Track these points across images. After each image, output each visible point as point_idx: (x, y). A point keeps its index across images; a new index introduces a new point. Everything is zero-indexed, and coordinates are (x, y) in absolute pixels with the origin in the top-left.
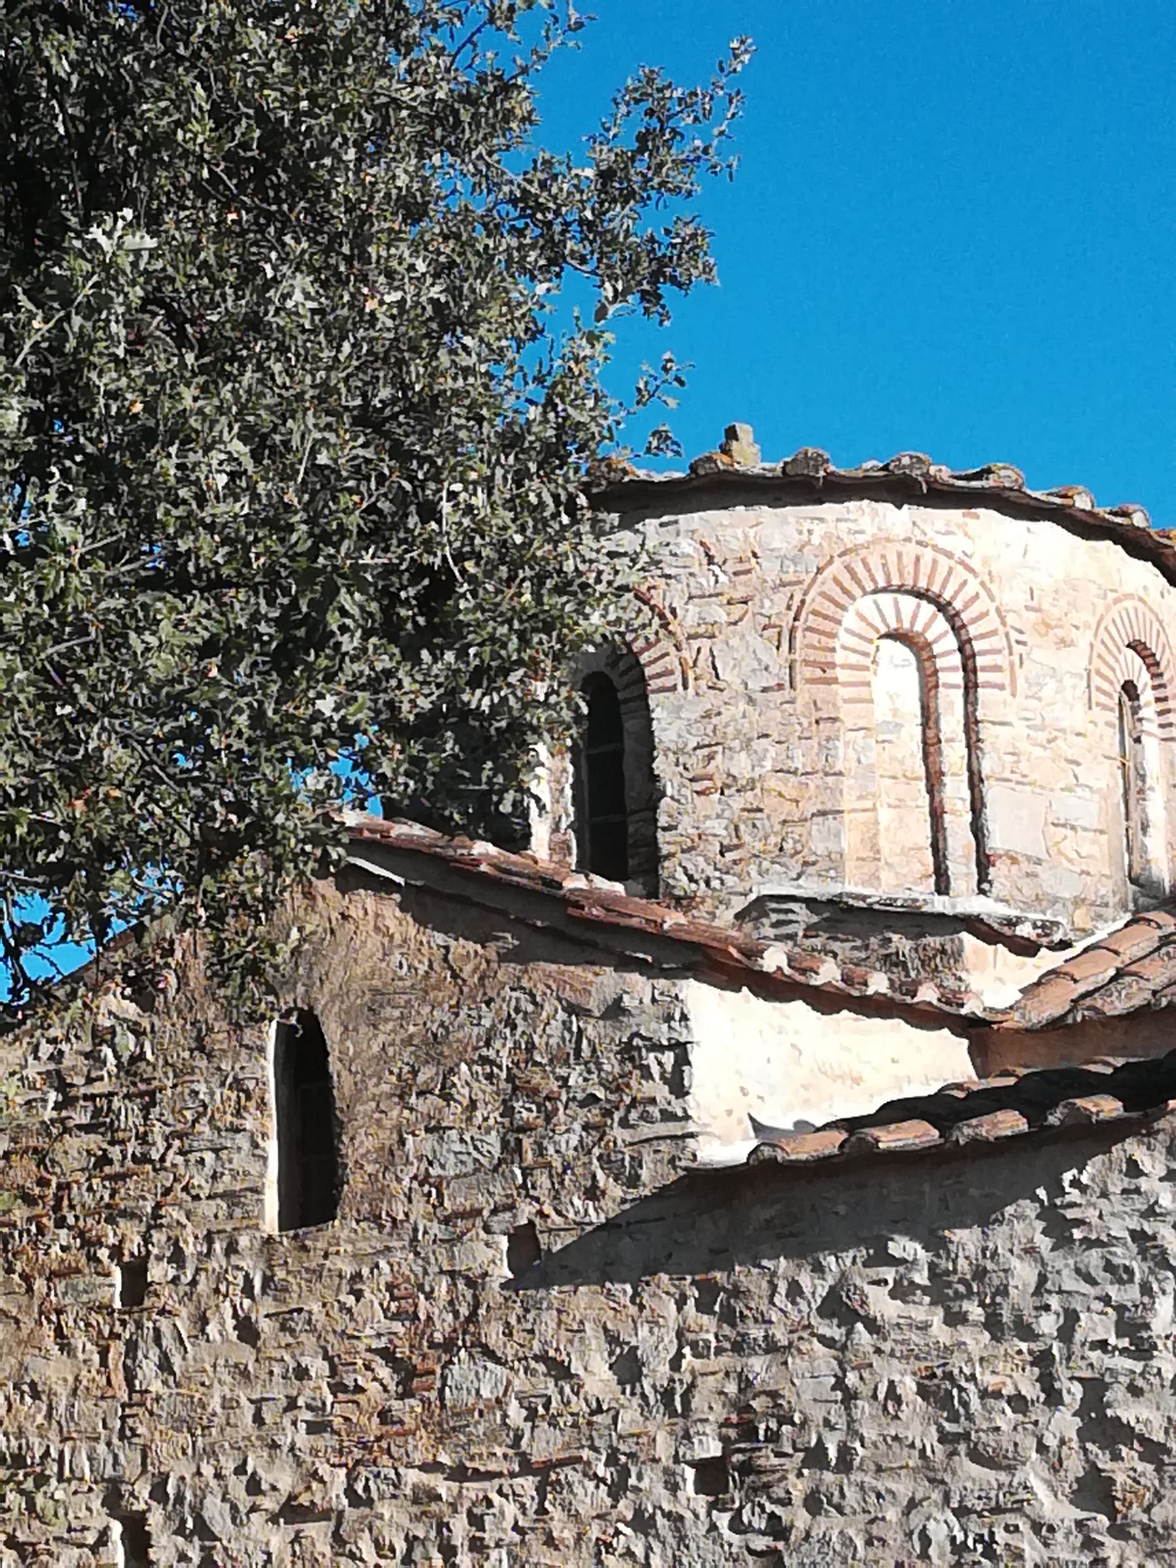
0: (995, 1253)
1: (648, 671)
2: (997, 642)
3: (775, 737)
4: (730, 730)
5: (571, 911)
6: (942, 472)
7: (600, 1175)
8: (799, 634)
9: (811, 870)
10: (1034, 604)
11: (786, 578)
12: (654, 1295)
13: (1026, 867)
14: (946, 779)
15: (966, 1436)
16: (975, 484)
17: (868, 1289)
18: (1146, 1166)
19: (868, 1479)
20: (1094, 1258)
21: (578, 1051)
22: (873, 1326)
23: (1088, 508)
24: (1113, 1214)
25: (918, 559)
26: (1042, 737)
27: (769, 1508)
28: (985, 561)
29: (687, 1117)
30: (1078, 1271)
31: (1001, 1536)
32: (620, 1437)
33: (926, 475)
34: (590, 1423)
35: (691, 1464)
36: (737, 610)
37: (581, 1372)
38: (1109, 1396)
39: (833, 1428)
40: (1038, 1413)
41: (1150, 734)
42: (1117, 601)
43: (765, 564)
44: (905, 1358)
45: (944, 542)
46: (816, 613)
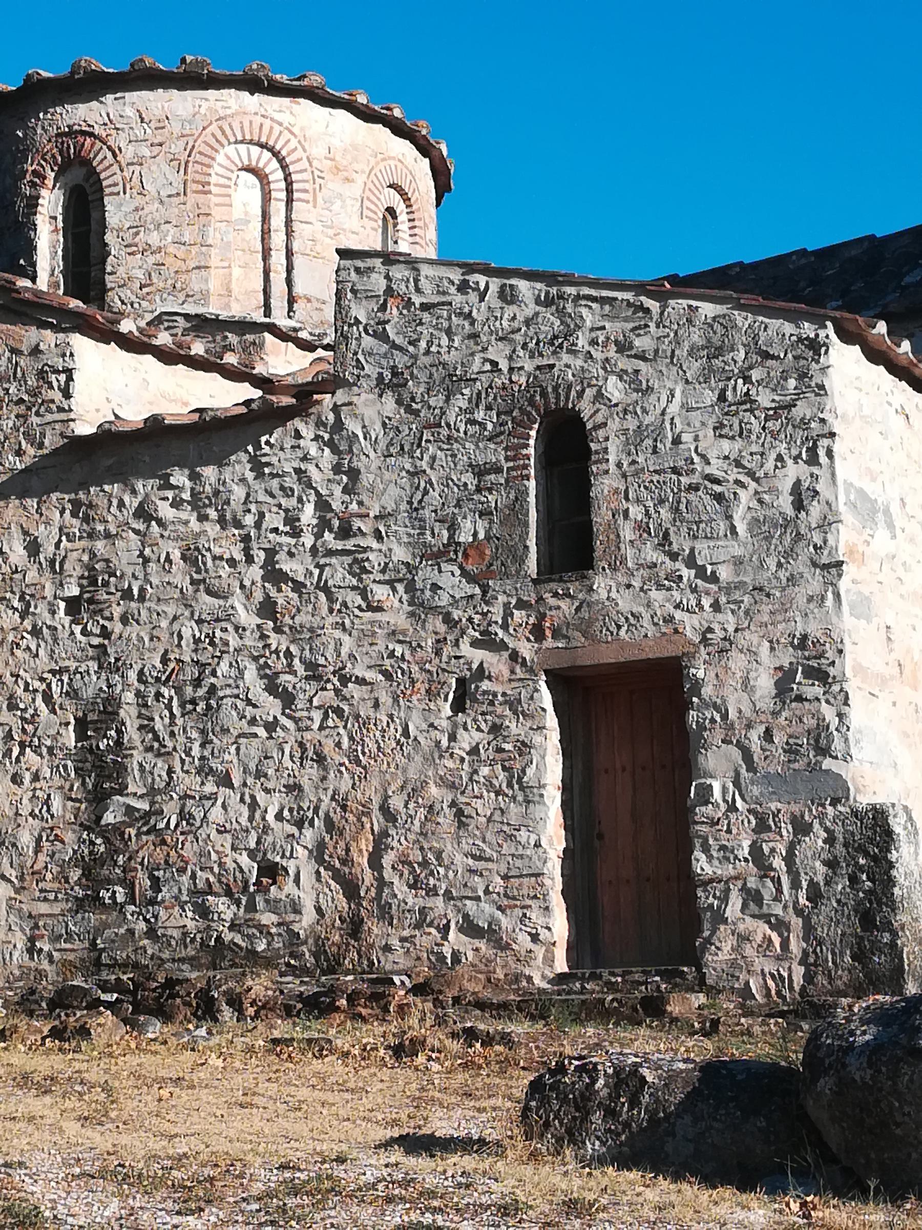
0: (224, 482)
1: (104, 183)
2: (306, 176)
3: (174, 223)
4: (150, 217)
5: (15, 295)
6: (282, 78)
7: (23, 443)
8: (190, 165)
9: (190, 299)
10: (331, 156)
11: (185, 132)
12: (48, 508)
13: (316, 305)
14: (272, 253)
15: (204, 580)
16: (295, 83)
17: (159, 502)
18: (304, 433)
19: (153, 605)
20: (275, 483)
21: (15, 373)
22: (161, 523)
23: (365, 102)
24: (286, 460)
25: (261, 125)
26: (331, 232)
27: (101, 622)
28: (302, 129)
29: (71, 410)
30: (266, 491)
31: (218, 633)
32: (27, 586)
33: (266, 76)
34: (11, 579)
35: (62, 599)
36: (156, 149)
37: (8, 551)
38: (277, 557)
39: (137, 579)
40: (242, 568)
41: (403, 239)
42: (383, 160)
43: (173, 124)
44: (176, 539)
45: (277, 116)
46: (200, 153)
